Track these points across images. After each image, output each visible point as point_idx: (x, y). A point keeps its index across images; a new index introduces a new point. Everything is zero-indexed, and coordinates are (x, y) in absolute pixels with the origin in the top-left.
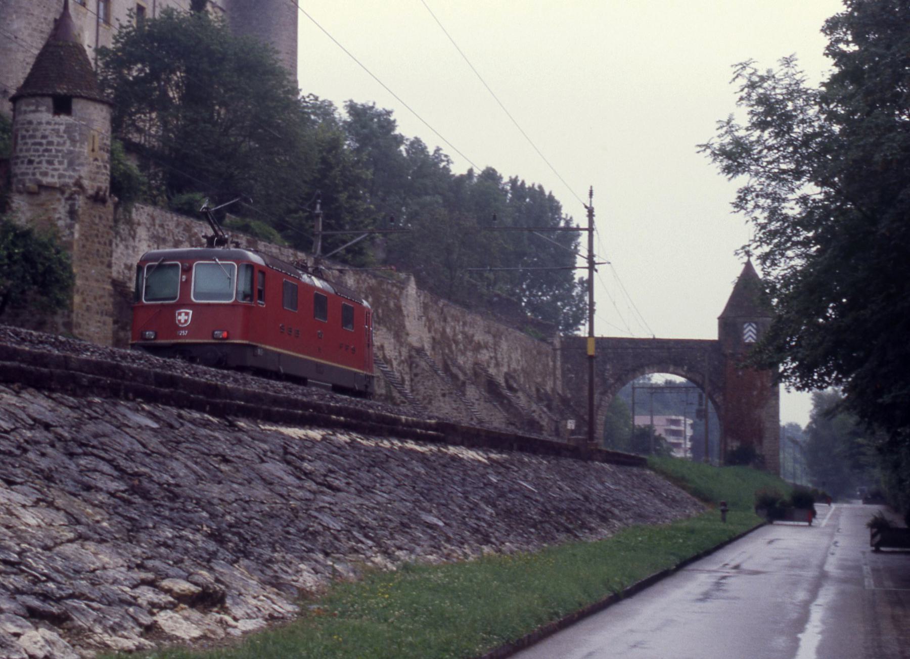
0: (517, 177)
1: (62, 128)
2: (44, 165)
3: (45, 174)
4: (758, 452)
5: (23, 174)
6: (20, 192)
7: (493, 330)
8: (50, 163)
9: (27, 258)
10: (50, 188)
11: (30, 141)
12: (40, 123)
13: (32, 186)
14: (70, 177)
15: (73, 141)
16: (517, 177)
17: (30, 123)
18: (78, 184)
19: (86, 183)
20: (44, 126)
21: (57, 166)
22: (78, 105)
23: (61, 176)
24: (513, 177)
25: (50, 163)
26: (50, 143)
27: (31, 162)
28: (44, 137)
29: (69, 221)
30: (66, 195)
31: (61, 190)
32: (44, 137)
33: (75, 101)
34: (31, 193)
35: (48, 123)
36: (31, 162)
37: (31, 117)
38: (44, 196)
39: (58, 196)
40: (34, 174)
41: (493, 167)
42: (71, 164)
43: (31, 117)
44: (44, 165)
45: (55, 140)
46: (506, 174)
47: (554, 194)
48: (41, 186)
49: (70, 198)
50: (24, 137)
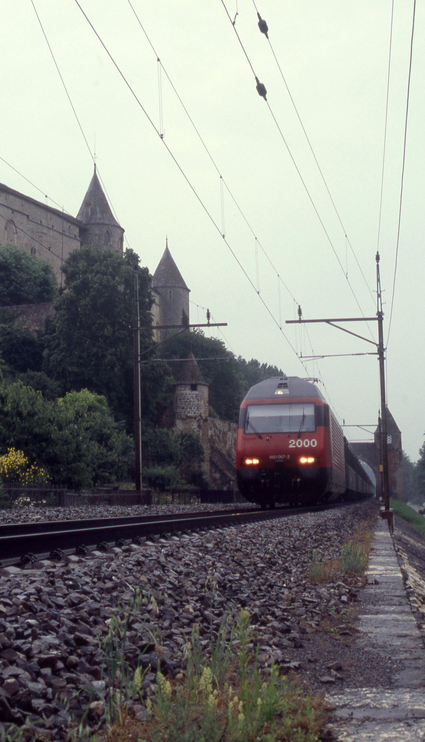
0: (266, 364)
1: (194, 396)
2: (189, 409)
3: (189, 412)
4: (394, 491)
5: (180, 412)
6: (179, 419)
7: (231, 459)
8: (190, 408)
9: (192, 445)
10: (190, 417)
11: (183, 401)
12: (186, 394)
13: (184, 417)
14: (198, 413)
15: (198, 400)
16: (266, 364)
17: (182, 394)
18: (200, 416)
19: (203, 415)
20: (188, 395)
21: (193, 409)
22: (199, 387)
23: (195, 413)
24: (265, 363)
25: (190, 408)
26: (190, 401)
27: (183, 408)
28: (188, 399)
29: (198, 429)
30: (197, 420)
31: (195, 418)
32: (188, 399)
33: (198, 386)
34: (183, 419)
35: (189, 394)
36: (183, 408)
37: (182, 392)
38: (188, 420)
39: (194, 420)
40: (185, 412)
41: (149, 269)
42: (198, 408)
43: (182, 392)
44: (189, 409)
45: (192, 400)
46: (261, 362)
47: (282, 370)
48: (188, 417)
49: (198, 421)
50: (180, 399)
